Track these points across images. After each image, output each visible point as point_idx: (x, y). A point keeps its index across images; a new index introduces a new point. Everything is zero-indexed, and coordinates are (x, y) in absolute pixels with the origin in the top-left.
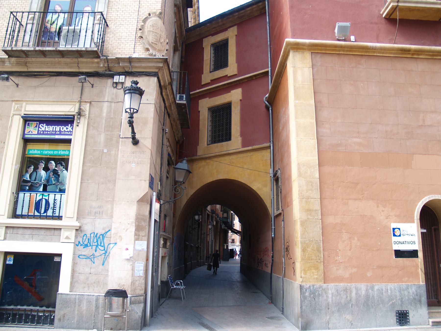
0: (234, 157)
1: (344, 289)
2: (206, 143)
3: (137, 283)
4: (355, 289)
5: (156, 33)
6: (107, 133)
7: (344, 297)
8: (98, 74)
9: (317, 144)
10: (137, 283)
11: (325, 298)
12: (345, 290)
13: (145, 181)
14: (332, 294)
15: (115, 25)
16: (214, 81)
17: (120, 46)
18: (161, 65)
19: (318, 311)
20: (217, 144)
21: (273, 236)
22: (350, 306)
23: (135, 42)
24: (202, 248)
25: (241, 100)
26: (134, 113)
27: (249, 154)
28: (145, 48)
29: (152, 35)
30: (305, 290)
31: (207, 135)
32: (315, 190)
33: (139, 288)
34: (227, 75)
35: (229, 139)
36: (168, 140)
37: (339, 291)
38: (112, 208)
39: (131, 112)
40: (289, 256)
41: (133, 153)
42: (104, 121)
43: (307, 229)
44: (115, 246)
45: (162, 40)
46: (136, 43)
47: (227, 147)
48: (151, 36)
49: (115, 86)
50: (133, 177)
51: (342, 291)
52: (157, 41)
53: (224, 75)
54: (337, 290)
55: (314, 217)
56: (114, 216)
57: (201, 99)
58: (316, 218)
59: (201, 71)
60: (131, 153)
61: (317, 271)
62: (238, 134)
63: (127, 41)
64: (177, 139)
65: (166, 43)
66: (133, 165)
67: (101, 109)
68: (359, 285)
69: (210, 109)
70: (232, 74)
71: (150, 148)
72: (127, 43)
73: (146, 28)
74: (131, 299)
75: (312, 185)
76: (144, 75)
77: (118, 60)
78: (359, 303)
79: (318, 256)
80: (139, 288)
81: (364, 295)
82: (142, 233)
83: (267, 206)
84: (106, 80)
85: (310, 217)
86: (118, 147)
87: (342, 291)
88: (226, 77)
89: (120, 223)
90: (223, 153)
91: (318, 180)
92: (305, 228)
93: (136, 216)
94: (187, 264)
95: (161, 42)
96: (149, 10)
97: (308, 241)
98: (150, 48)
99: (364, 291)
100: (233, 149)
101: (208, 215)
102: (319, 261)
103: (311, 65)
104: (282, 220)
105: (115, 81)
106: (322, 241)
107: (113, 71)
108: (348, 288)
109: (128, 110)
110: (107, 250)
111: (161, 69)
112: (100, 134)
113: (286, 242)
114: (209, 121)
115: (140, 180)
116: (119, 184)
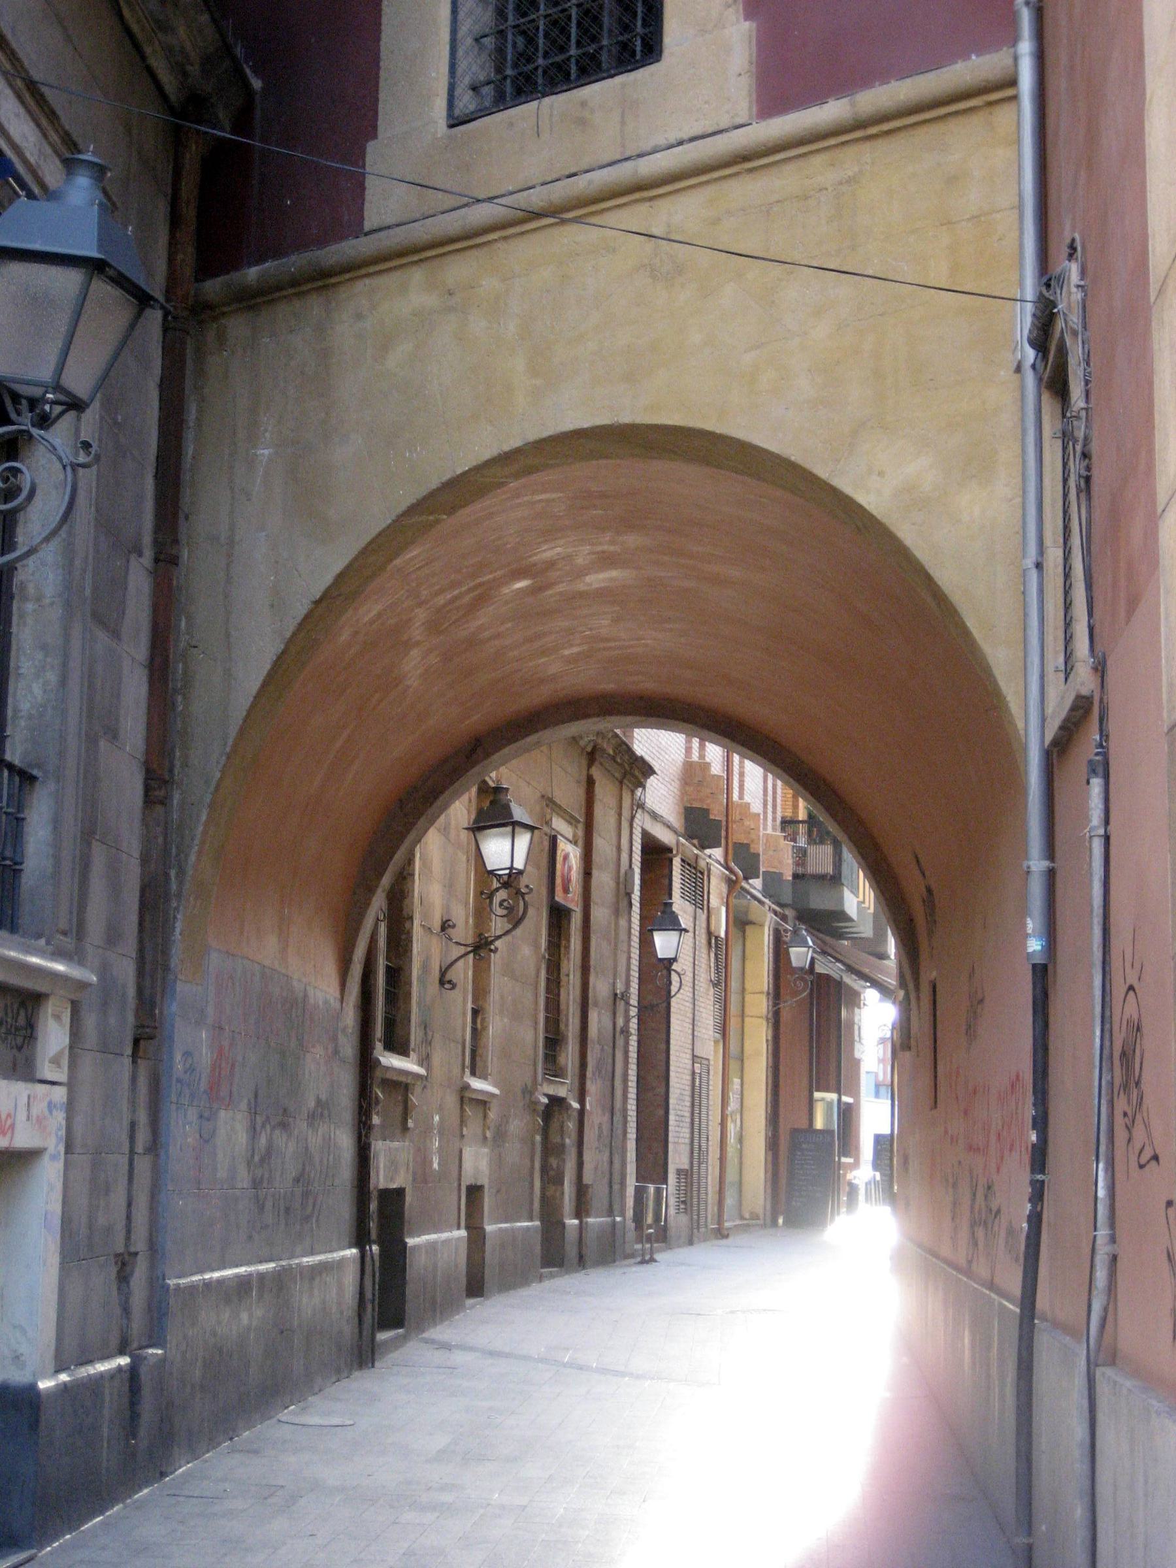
2: (440, 105)
20: (535, 104)
21: (1035, 945)
24: (596, 1118)
31: (445, 35)
40: (1139, 1133)
47: (623, 123)
83: (991, 660)
90: (581, 185)
94: (411, 1241)
100: (673, 137)
104: (1093, 772)
113: (1119, 989)
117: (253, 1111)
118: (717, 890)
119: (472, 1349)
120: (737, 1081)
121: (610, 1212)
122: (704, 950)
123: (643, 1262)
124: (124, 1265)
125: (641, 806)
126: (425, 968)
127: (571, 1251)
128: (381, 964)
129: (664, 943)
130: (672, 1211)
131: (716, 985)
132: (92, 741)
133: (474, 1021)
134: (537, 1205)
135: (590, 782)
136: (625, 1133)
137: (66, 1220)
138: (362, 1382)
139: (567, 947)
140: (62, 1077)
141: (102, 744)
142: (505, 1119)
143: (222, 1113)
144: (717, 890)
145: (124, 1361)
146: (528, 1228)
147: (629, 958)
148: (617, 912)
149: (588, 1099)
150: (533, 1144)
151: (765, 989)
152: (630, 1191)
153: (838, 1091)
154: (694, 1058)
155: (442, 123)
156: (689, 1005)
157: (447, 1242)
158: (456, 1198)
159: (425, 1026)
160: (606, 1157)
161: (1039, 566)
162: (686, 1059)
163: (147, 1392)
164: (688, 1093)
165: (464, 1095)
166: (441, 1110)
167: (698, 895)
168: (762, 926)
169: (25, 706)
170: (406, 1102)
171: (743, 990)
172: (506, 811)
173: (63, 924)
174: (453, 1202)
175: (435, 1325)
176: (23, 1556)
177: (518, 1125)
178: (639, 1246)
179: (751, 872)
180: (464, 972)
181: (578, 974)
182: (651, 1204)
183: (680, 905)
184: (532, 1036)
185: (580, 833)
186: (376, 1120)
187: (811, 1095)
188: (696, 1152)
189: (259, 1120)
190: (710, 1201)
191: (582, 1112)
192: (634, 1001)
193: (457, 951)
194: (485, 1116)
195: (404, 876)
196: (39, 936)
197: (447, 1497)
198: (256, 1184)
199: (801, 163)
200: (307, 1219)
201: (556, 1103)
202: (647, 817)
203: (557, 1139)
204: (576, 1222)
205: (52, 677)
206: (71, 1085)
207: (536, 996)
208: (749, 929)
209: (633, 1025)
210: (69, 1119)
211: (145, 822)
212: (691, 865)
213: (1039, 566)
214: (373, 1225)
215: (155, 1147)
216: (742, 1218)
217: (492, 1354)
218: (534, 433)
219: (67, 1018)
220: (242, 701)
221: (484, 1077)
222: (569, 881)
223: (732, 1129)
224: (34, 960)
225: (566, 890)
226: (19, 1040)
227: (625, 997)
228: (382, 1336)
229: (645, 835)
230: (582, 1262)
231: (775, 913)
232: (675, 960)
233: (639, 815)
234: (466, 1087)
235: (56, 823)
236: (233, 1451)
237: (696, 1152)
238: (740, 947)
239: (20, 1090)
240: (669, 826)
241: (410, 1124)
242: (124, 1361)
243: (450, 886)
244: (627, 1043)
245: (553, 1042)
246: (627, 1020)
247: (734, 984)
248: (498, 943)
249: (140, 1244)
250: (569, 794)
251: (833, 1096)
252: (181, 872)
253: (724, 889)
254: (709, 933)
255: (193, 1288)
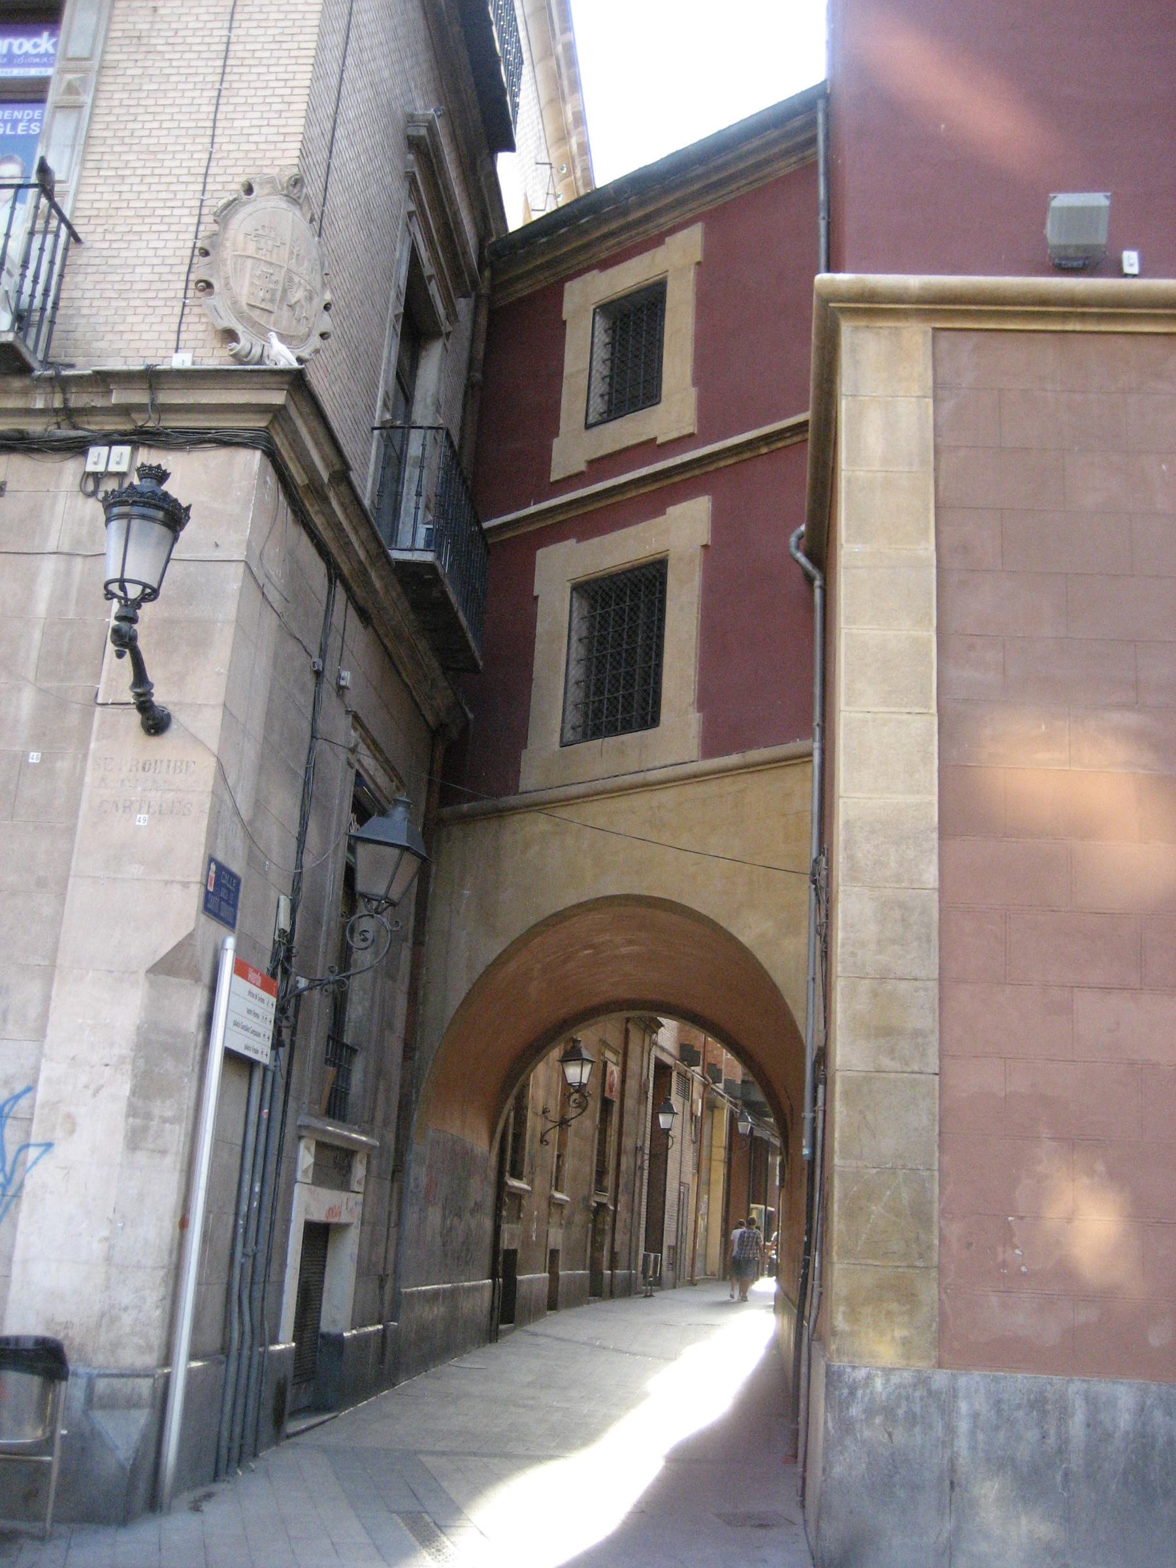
0: (667, 797)
1: (1032, 1397)
3: (127, 1319)
4: (1083, 1404)
5: (271, 264)
6: (46, 685)
7: (1032, 1435)
8: (23, 438)
9: (936, 737)
10: (127, 1319)
11: (939, 1429)
12: (1038, 1404)
13: (185, 885)
14: (975, 1416)
15: (108, 237)
16: (600, 466)
17: (124, 322)
18: (278, 398)
19: (902, 1494)
21: (806, 1151)
22: (1059, 1478)
23: (184, 305)
24: (623, 1214)
25: (705, 547)
26: (137, 603)
27: (728, 785)
28: (220, 328)
29: (252, 276)
30: (846, 1391)
32: (915, 944)
33: (136, 1339)
34: (655, 439)
35: (649, 718)
36: (356, 718)
37: (1005, 1407)
38: (47, 999)
39: (126, 593)
41: (144, 768)
42: (37, 635)
43: (870, 1117)
44: (46, 1157)
45: (298, 295)
46: (187, 310)
48: (248, 275)
49: (90, 487)
50: (135, 870)
51: (1019, 1406)
52: (272, 301)
53: (644, 438)
54: (999, 1401)
55: (907, 1065)
56: (49, 1032)
57: (546, 546)
58: (916, 1069)
59: (549, 422)
60: (134, 768)
61: (908, 1307)
62: (690, 695)
63: (151, 303)
64: (430, 718)
65: (318, 304)
66: (142, 820)
67: (29, 582)
68: (1102, 1387)
69: (581, 589)
70: (674, 435)
71: (214, 747)
72: (150, 311)
73: (228, 244)
74: (90, 1386)
75: (903, 920)
76: (210, 441)
77: (104, 379)
78: (1099, 1468)
79: (918, 1238)
80: (136, 1339)
81: (1127, 1433)
82: (163, 1108)
83: (796, 1018)
84: (57, 465)
85: (886, 1062)
86: (84, 743)
87: (1019, 1406)
88: (650, 449)
89: (73, 1058)
90: (620, 781)
91: (936, 896)
92: (861, 1112)
93: (138, 1034)
94: (519, 1278)
95: (293, 301)
96: (248, 170)
97: (875, 1171)
98: (239, 329)
99: (1127, 1416)
100: (663, 764)
101: (663, 1070)
102: (919, 1263)
103: (930, 383)
105: (90, 468)
106: (936, 1174)
107: (87, 427)
108: (1049, 1395)
109: (115, 588)
110: (13, 1171)
111: (283, 418)
112: (20, 690)
114: (574, 638)
115: (166, 883)
116: (79, 894)
117: (444, 1208)
118: (697, 1090)
119: (549, 1336)
120: (706, 1197)
121: (629, 1268)
122: (689, 1123)
123: (646, 1296)
124: (382, 1281)
125: (656, 1044)
126: (533, 1136)
127: (606, 1289)
128: (511, 1131)
129: (664, 1120)
130: (664, 1269)
131: (694, 1143)
132: (382, 1031)
133: (558, 1162)
134: (588, 1261)
135: (627, 1031)
136: (639, 1224)
137: (359, 1256)
138: (491, 1349)
139: (611, 1121)
140: (361, 1190)
141: (386, 1032)
142: (573, 1214)
143: (430, 1209)
144: (697, 1090)
145: (380, 1327)
146: (583, 1274)
147: (645, 1127)
148: (639, 1103)
149: (619, 1205)
150: (587, 1228)
151: (724, 1144)
152: (641, 1257)
153: (765, 1205)
154: (681, 1183)
155: (557, 745)
156: (678, 1153)
157: (539, 1278)
158: (543, 1259)
159: (532, 1166)
160: (628, 1237)
161: (814, 979)
162: (676, 1185)
163: (389, 1340)
164: (676, 1203)
165: (552, 1202)
166: (538, 1209)
167: (686, 1093)
168: (723, 1109)
169: (353, 1016)
170: (520, 1203)
171: (711, 1146)
172: (579, 1053)
173: (366, 1118)
174: (542, 1258)
175: (530, 1323)
176: (333, 1415)
177: (579, 1218)
178: (644, 1288)
179: (717, 1079)
180: (554, 1136)
181: (616, 1136)
182: (652, 1265)
183: (676, 1100)
184: (588, 1170)
185: (620, 1059)
186: (504, 1213)
187: (749, 1205)
188: (680, 1236)
189: (447, 1212)
190: (687, 1264)
191: (615, 1211)
192: (647, 1151)
193: (550, 1125)
194: (562, 1212)
195: (525, 1086)
196: (355, 1124)
197: (531, 1402)
198: (444, 1245)
199: (719, 781)
200: (467, 1263)
201: (601, 1206)
202: (658, 1049)
203: (600, 1226)
204: (609, 1272)
205: (367, 1004)
206: (364, 1193)
207: (592, 1147)
208: (716, 1112)
209: (646, 1163)
210: (363, 1209)
211: (403, 1067)
212: (683, 1076)
213: (814, 979)
214: (500, 1268)
215: (399, 1223)
216: (706, 1274)
217: (558, 1339)
218: (593, 895)
219: (365, 1162)
220: (451, 1012)
221: (562, 1192)
222: (613, 1085)
223: (701, 1223)
224: (354, 1136)
225: (611, 1091)
226: (344, 1172)
227: (642, 1149)
228: (502, 1327)
229: (656, 1058)
230: (612, 1295)
231: (731, 1102)
232: (669, 1129)
233: (654, 1048)
234: (552, 1197)
235: (365, 1073)
236: (426, 1377)
237: (680, 1236)
238: (710, 1121)
239: (345, 1195)
240: (671, 1055)
241: (522, 1216)
242: (380, 1327)
243: (548, 1091)
244: (642, 1175)
245: (601, 1173)
246: (643, 1162)
247: (705, 1142)
248: (572, 1122)
249: (390, 1271)
250: (615, 1039)
251: (763, 1207)
252: (418, 1092)
253: (701, 1089)
254: (692, 1114)
255: (412, 1294)
